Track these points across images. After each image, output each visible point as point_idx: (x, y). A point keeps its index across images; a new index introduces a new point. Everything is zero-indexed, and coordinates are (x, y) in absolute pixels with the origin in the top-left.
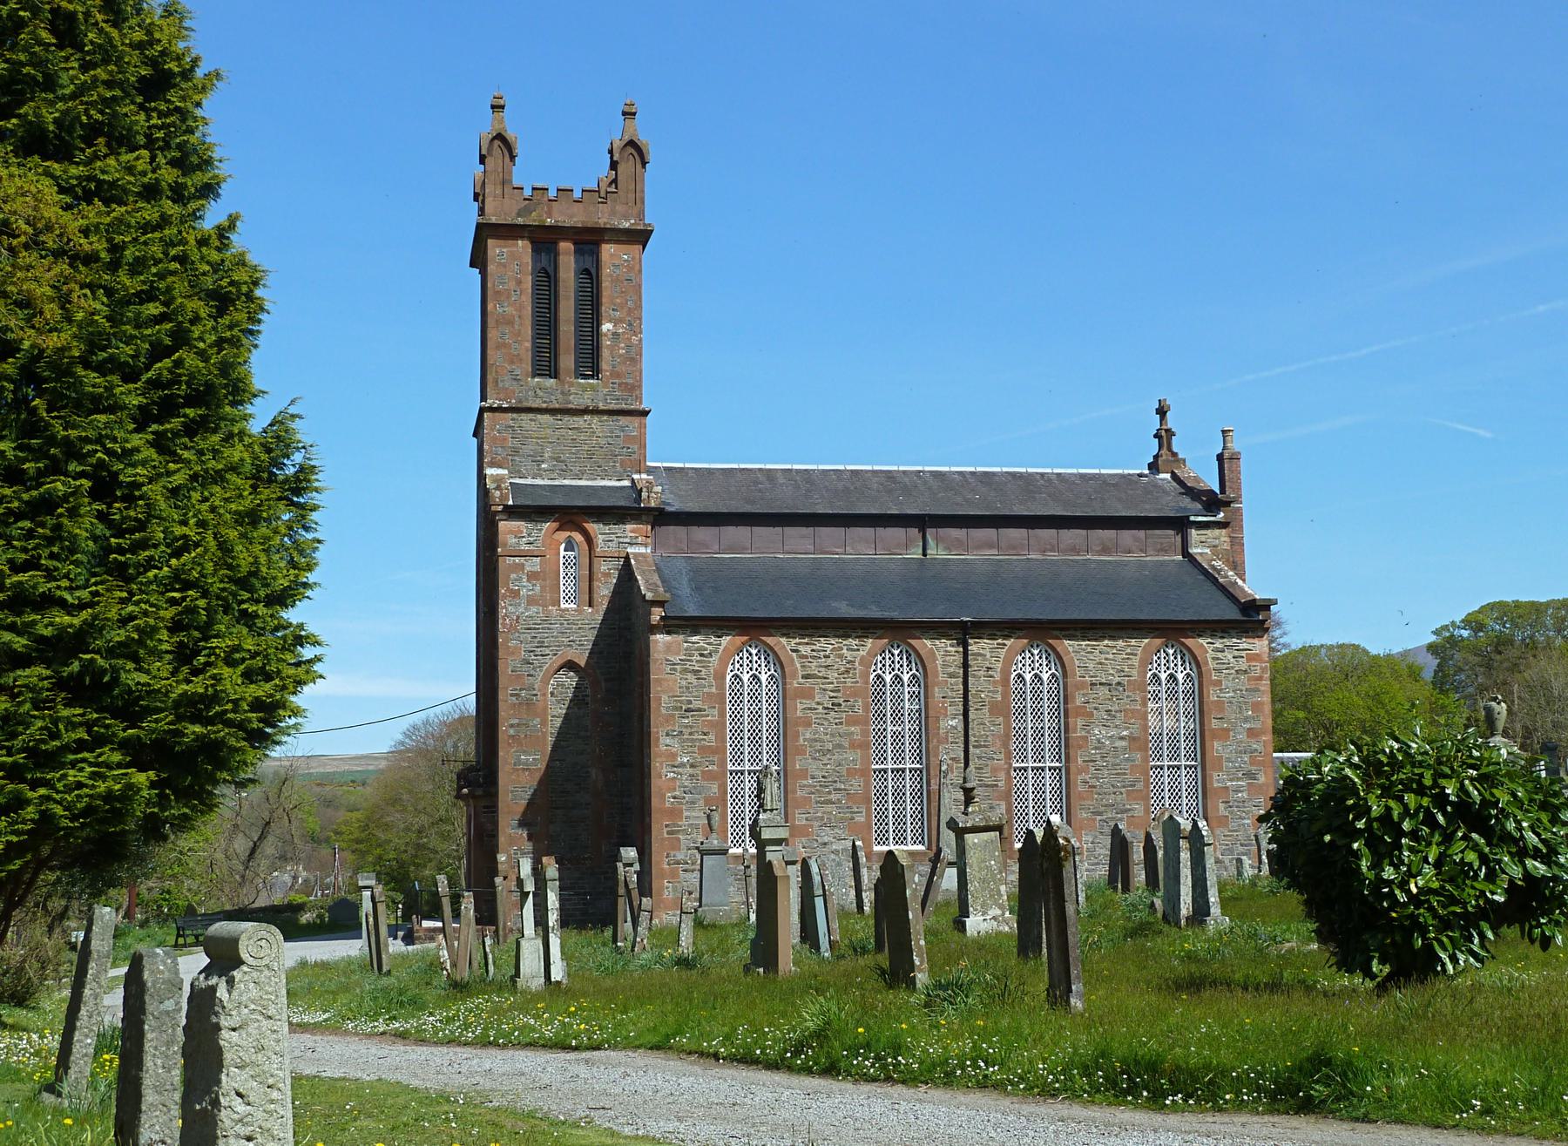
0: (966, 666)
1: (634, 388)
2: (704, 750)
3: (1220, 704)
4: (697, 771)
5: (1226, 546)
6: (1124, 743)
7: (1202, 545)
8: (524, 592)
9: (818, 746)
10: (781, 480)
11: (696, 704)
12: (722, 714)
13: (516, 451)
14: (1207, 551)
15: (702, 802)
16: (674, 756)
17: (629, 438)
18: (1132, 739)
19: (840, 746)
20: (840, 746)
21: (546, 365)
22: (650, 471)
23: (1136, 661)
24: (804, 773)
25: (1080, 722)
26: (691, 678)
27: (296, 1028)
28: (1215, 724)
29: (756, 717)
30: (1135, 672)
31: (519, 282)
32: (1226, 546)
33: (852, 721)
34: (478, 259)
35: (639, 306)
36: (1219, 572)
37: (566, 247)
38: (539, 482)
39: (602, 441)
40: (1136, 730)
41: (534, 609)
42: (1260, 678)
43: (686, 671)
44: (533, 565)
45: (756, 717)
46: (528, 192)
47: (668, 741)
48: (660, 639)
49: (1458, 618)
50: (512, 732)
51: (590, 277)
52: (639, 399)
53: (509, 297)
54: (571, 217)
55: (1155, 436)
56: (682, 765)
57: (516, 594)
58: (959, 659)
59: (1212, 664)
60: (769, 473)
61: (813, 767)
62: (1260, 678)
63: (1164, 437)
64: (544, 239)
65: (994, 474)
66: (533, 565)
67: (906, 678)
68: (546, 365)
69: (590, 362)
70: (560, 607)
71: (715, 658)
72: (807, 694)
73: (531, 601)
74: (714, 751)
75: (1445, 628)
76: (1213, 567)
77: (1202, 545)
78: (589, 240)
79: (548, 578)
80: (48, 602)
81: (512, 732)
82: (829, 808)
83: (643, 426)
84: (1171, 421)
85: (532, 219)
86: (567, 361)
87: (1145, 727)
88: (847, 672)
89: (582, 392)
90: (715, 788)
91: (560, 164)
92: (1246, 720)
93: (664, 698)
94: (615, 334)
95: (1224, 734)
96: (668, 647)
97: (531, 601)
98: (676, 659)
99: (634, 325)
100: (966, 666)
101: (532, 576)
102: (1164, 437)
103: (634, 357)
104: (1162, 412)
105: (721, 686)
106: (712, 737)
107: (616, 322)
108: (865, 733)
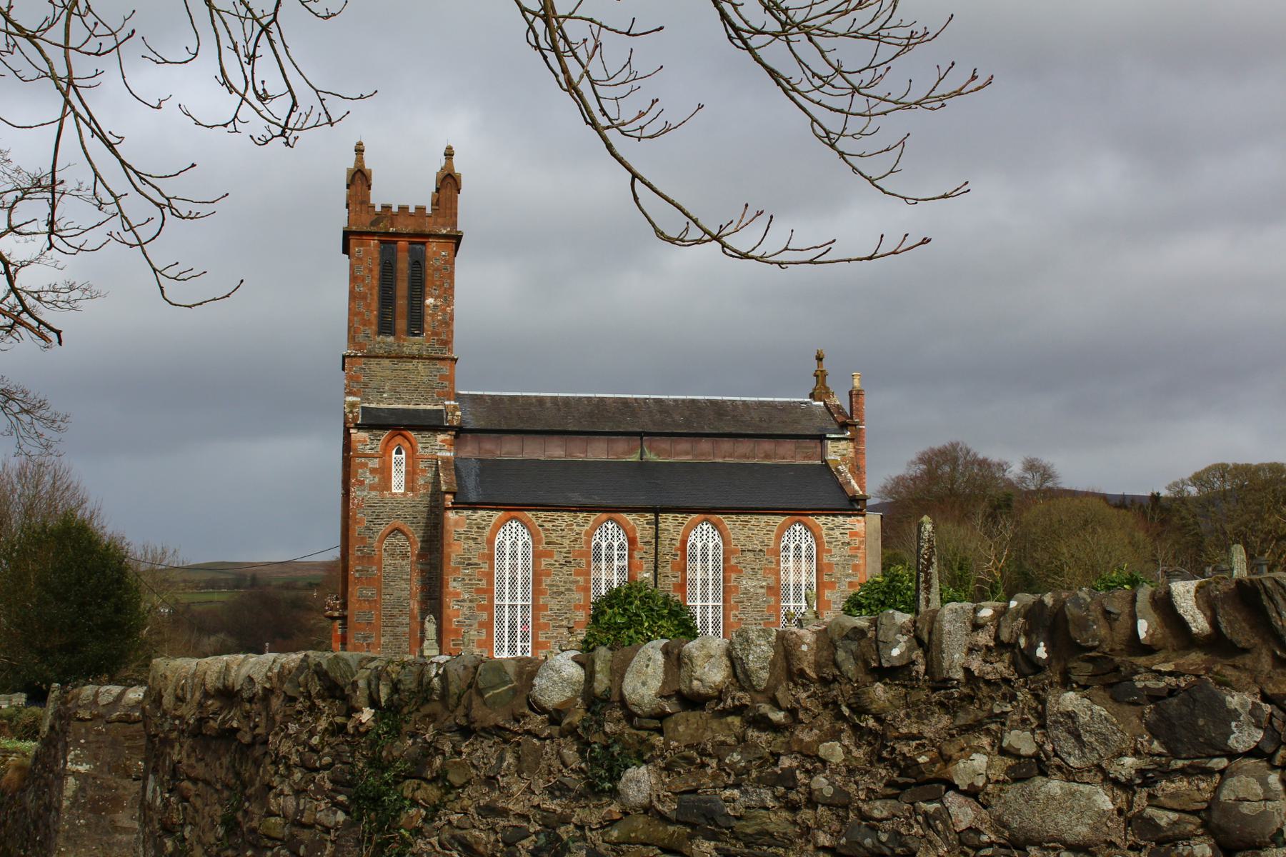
0: (657, 537)
1: (447, 343)
2: (479, 591)
3: (830, 565)
4: (474, 605)
5: (852, 455)
6: (763, 591)
7: (837, 451)
8: (367, 481)
9: (555, 589)
10: (548, 405)
11: (474, 560)
12: (492, 567)
13: (366, 385)
14: (839, 458)
15: (476, 625)
16: (458, 594)
17: (443, 378)
18: (769, 588)
19: (569, 590)
20: (569, 590)
21: (386, 327)
22: (458, 397)
23: (773, 535)
24: (545, 607)
25: (733, 576)
26: (471, 543)
27: (344, 641)
28: (826, 579)
29: (513, 568)
30: (772, 543)
31: (371, 270)
32: (852, 455)
33: (578, 574)
34: (346, 250)
35: (452, 287)
36: (840, 473)
37: (403, 244)
38: (382, 406)
39: (425, 379)
40: (772, 581)
41: (373, 493)
42: (858, 548)
43: (468, 538)
44: (374, 463)
45: (513, 568)
46: (378, 209)
47: (455, 584)
48: (451, 515)
49: (1188, 473)
50: (357, 575)
51: (418, 264)
52: (450, 350)
53: (363, 281)
54: (407, 227)
55: (816, 375)
56: (464, 601)
57: (362, 483)
58: (652, 532)
59: (825, 539)
60: (541, 401)
61: (553, 604)
62: (858, 548)
63: (820, 376)
64: (388, 240)
65: (698, 401)
66: (374, 463)
67: (616, 545)
68: (386, 327)
69: (416, 323)
70: (398, 475)
71: (488, 529)
72: (549, 554)
73: (372, 488)
74: (485, 591)
75: (1176, 484)
76: (838, 470)
77: (837, 451)
78: (420, 238)
79: (384, 473)
80: (373, 659)
81: (357, 575)
82: (561, 630)
83: (452, 368)
84: (826, 365)
85: (381, 227)
86: (401, 324)
87: (778, 580)
88: (576, 540)
89: (413, 345)
90: (485, 616)
91: (403, 186)
92: (848, 575)
93: (453, 555)
94: (435, 306)
95: (832, 585)
96: (456, 523)
97: (372, 488)
98: (461, 530)
99: (447, 294)
100: (657, 537)
101: (373, 471)
102: (820, 376)
103: (448, 322)
104: (819, 359)
105: (492, 548)
106: (484, 582)
107: (436, 298)
108: (588, 581)
